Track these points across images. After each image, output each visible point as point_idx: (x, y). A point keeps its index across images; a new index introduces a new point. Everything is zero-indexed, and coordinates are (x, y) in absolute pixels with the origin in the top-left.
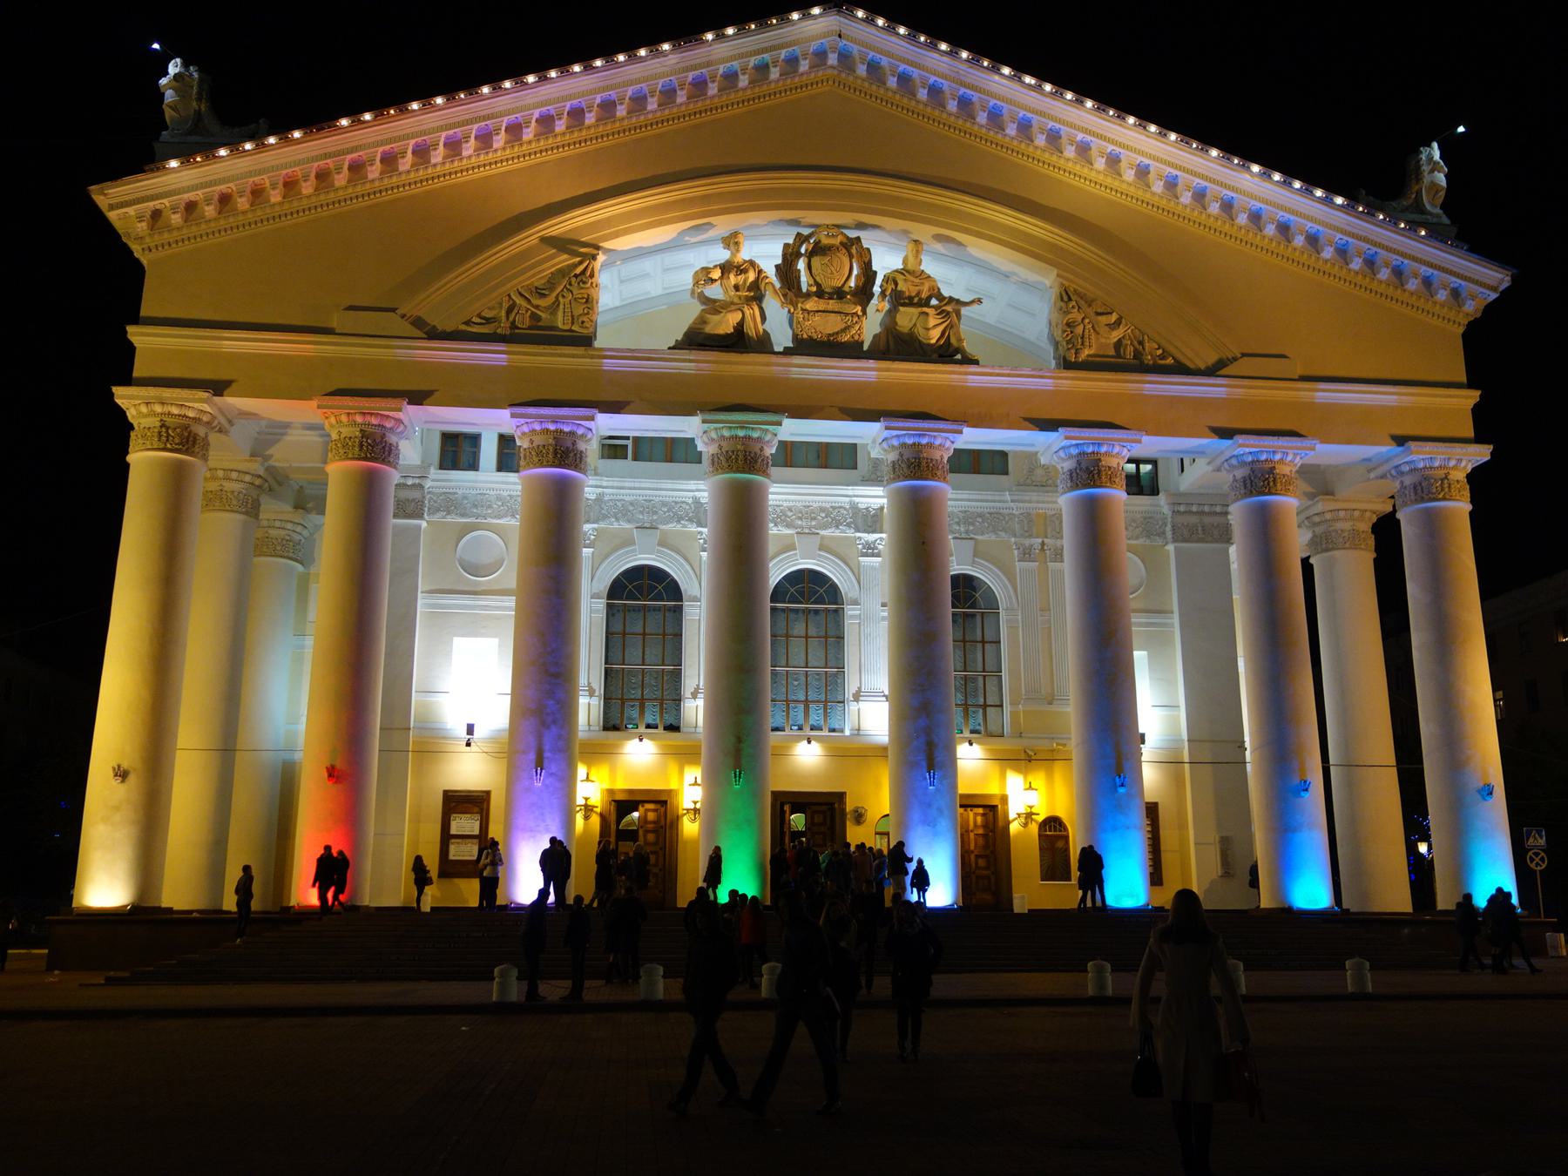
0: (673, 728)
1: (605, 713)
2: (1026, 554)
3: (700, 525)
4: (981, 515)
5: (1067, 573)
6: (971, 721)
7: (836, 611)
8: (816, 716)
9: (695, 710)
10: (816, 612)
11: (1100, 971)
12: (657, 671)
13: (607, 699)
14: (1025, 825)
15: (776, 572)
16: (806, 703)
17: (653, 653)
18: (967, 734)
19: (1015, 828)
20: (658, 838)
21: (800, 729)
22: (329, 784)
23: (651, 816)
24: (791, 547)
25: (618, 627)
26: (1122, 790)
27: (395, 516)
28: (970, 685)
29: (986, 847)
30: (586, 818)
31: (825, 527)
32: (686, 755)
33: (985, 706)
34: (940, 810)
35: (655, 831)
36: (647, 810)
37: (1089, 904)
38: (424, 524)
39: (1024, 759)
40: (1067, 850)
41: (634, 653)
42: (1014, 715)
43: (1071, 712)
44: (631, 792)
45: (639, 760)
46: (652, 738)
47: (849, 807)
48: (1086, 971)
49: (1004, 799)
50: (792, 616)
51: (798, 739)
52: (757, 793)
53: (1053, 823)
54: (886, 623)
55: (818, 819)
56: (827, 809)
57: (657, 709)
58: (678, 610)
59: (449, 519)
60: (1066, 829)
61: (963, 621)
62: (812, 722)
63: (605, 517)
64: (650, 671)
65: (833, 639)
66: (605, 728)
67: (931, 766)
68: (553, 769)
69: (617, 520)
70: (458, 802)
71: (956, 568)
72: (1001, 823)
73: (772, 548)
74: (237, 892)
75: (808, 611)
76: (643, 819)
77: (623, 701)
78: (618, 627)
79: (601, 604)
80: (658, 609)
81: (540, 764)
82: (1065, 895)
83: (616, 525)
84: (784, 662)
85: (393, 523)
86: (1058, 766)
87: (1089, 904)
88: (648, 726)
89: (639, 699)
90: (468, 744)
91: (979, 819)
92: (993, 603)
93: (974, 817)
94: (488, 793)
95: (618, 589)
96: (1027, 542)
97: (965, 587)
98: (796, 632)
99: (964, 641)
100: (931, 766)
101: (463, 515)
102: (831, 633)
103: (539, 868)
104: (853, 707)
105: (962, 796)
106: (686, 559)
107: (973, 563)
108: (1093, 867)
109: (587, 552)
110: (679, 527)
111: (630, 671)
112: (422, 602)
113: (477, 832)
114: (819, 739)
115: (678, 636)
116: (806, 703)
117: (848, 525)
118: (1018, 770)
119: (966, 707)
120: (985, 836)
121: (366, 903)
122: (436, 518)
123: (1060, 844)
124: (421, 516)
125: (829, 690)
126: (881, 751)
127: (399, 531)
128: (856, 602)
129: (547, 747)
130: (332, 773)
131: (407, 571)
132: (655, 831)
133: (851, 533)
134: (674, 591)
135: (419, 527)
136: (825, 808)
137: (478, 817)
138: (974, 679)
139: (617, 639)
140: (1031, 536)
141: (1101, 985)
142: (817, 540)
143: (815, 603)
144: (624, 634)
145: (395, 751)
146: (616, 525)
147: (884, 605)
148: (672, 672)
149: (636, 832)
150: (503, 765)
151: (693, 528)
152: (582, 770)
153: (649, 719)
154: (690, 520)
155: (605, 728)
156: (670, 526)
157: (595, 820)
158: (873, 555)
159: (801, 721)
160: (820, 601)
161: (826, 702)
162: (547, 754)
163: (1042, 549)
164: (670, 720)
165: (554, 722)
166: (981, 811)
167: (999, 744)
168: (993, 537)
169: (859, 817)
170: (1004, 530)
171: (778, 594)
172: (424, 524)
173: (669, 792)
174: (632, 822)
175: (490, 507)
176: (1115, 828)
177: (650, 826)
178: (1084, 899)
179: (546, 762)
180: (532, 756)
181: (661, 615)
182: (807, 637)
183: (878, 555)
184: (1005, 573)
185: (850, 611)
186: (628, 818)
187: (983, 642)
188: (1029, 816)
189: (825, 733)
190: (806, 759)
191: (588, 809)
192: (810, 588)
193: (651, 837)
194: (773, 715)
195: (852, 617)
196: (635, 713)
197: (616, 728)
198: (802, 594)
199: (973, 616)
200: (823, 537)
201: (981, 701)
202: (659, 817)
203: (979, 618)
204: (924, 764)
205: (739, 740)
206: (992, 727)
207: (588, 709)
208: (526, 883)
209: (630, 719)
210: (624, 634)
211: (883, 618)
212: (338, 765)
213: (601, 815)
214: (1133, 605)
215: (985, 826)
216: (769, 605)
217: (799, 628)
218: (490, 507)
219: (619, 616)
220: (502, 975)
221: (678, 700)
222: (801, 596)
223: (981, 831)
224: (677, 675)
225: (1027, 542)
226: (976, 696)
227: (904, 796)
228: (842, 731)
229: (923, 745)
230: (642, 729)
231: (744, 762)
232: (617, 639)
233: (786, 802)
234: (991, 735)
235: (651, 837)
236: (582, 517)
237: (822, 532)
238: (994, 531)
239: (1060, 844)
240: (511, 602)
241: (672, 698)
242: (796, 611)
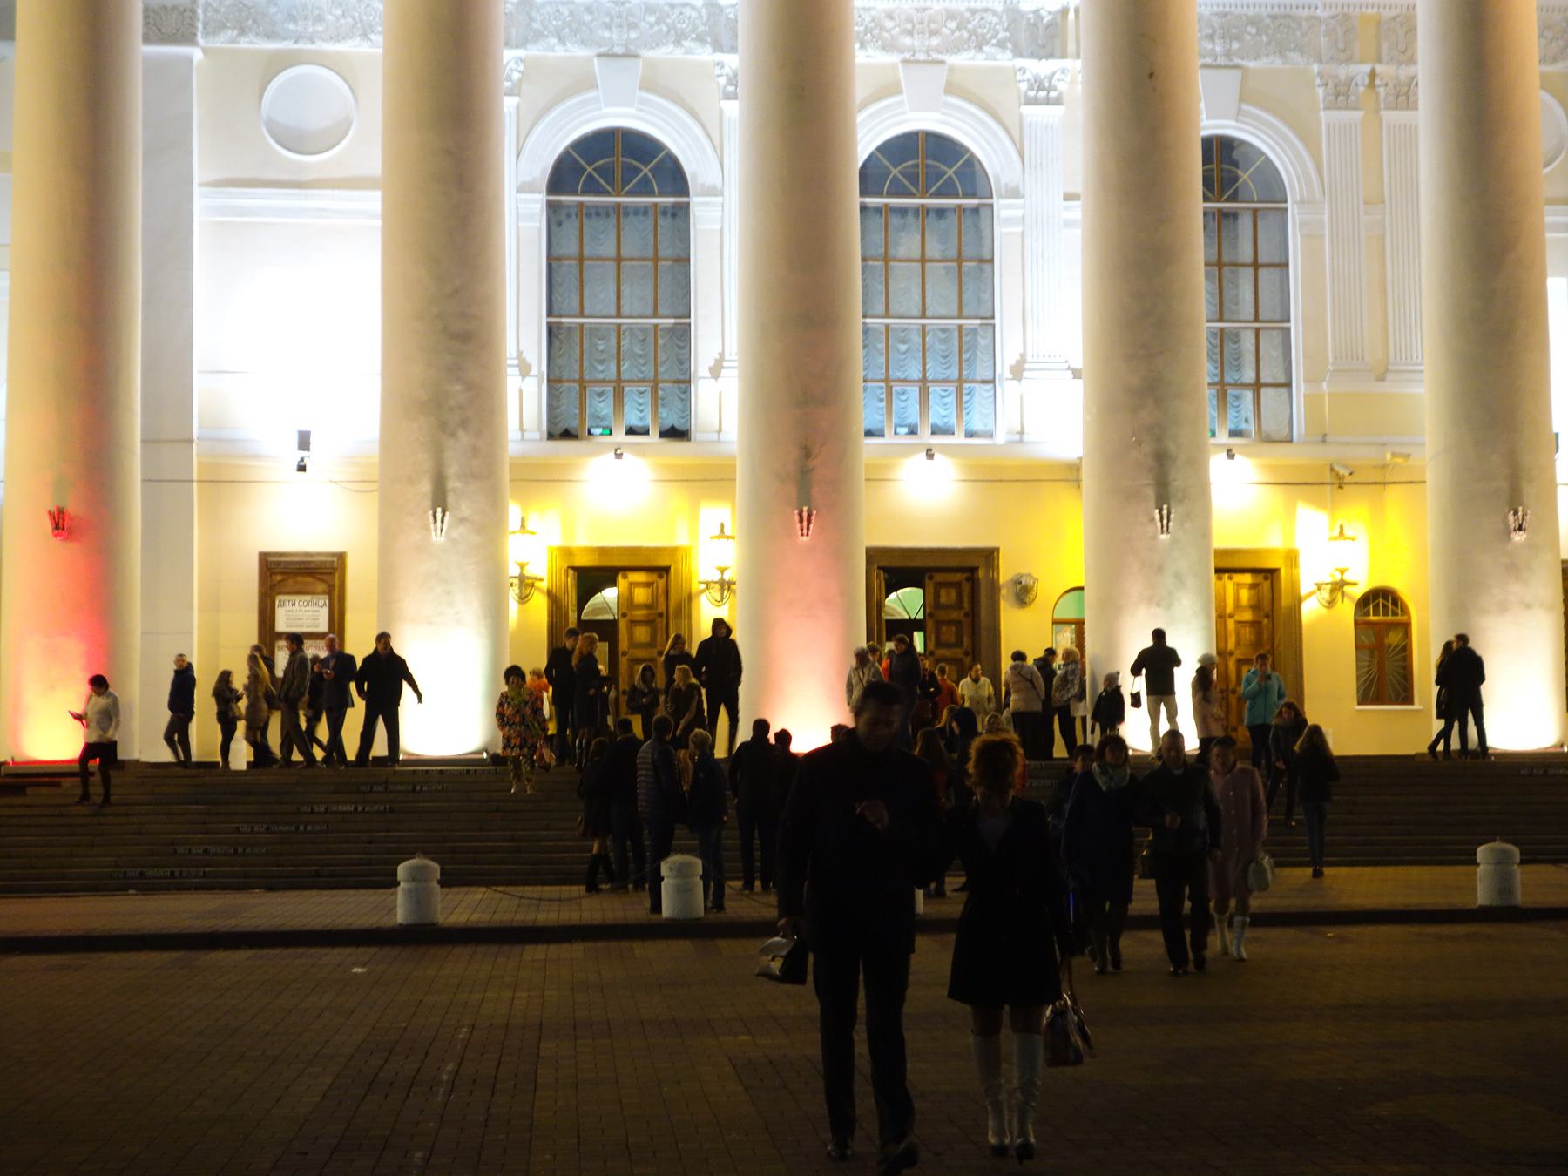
0: (676, 433)
1: (551, 408)
2: (1341, 95)
3: (718, 47)
4: (1254, 21)
5: (1423, 133)
6: (1231, 413)
7: (976, 210)
8: (941, 408)
9: (722, 399)
10: (941, 212)
11: (1502, 860)
12: (643, 329)
13: (554, 382)
14: (1331, 603)
15: (870, 132)
16: (924, 383)
17: (637, 293)
18: (1223, 438)
19: (1311, 611)
20: (654, 634)
21: (913, 431)
22: (56, 543)
23: (641, 595)
24: (893, 89)
25: (570, 247)
26: (1518, 537)
27: (147, 40)
28: (1229, 347)
29: (1257, 643)
30: (523, 599)
31: (958, 48)
32: (709, 480)
33: (1257, 386)
34: (1178, 577)
35: (649, 622)
36: (632, 585)
37: (1455, 744)
38: (197, 54)
39: (1334, 482)
40: (1405, 651)
41: (601, 293)
42: (1312, 402)
43: (1423, 395)
44: (603, 551)
45: (614, 498)
46: (640, 451)
47: (1005, 574)
48: (1475, 863)
49: (1292, 557)
50: (895, 221)
51: (910, 450)
52: (838, 553)
53: (1381, 600)
54: (1078, 232)
55: (948, 596)
56: (960, 584)
57: (648, 398)
58: (681, 213)
59: (244, 44)
60: (1405, 611)
61: (1221, 222)
62: (934, 418)
63: (538, 36)
64: (631, 328)
65: (972, 262)
66: (551, 436)
67: (1163, 496)
68: (466, 509)
69: (562, 41)
70: (280, 574)
71: (1211, 125)
72: (1285, 601)
73: (860, 88)
74: (1438, 682)
75: (924, 212)
76: (627, 602)
77: (583, 384)
78: (570, 247)
79: (536, 203)
80: (644, 211)
81: (440, 501)
82: (1411, 729)
83: (560, 52)
84: (881, 309)
85: (142, 54)
86: (1393, 493)
87: (1455, 744)
88: (631, 431)
89: (615, 375)
90: (302, 468)
91: (1245, 595)
92: (1273, 188)
93: (1239, 590)
94: (341, 557)
95: (566, 175)
96: (1343, 72)
97: (1222, 156)
98: (902, 252)
99: (1220, 264)
100: (1163, 496)
101: (270, 36)
102: (967, 253)
103: (1194, 674)
104: (1008, 390)
105: (1221, 553)
106: (694, 115)
107: (1239, 115)
108: (1462, 674)
109: (509, 104)
110: (678, 53)
111: (594, 330)
112: (203, 204)
113: (323, 627)
114: (948, 450)
115: (683, 260)
116: (924, 383)
117: (1001, 45)
118: (1318, 502)
119: (1222, 389)
120: (1255, 624)
121: (136, 756)
122: (220, 42)
123: (1393, 638)
124: (190, 39)
125: (964, 358)
126: (1070, 473)
127: (156, 68)
128: (1015, 193)
129: (452, 470)
130: (60, 523)
131: (173, 143)
132: (649, 622)
133: (1005, 60)
134: (673, 177)
135: (189, 60)
136: (958, 577)
137: (324, 600)
138: (1236, 337)
139: (569, 269)
140: (1349, 60)
141: (1504, 884)
142: (940, 74)
143: (938, 194)
144: (581, 259)
145: (168, 483)
146: (560, 52)
147: (1068, 197)
148: (672, 330)
149: (613, 624)
150: (371, 505)
151: (705, 55)
152: (514, 510)
153: (632, 417)
154: (701, 39)
155: (551, 436)
156: (665, 53)
157: (539, 607)
158: (1048, 101)
159: (913, 416)
160: (947, 191)
161: (960, 381)
162: (453, 484)
163: (1372, 85)
164: (670, 419)
165: (464, 424)
166: (1247, 578)
167: (1283, 456)
168: (1278, 63)
169: (1023, 593)
170: (1300, 49)
171: (870, 178)
172: (197, 54)
173: (673, 551)
174: (606, 608)
175: (319, 19)
176: (1503, 608)
177: (640, 614)
178: (1445, 734)
179: (451, 499)
180: (426, 487)
181: (650, 221)
182: (923, 260)
183: (1058, 101)
184: (1303, 139)
185: (1004, 209)
186: (597, 599)
187: (1256, 265)
188: (1338, 587)
189: (959, 439)
190: (919, 495)
191: (526, 585)
192: (930, 170)
193: (642, 634)
194: (867, 410)
195: (1009, 221)
196: (605, 407)
197: (567, 435)
198: (913, 179)
199: (1234, 215)
200: (952, 69)
201: (1249, 376)
202: (655, 597)
203: (1245, 223)
204: (1150, 493)
205: (807, 453)
206: (1269, 425)
207: (523, 398)
208: (447, 720)
209: (598, 418)
210: (581, 259)
211: (1068, 224)
212: (73, 507)
213: (550, 595)
214: (1548, 190)
215: (1256, 607)
216: (856, 200)
217: (908, 244)
218: (319, 19)
219: (570, 228)
220: (415, 876)
221: (684, 383)
222: (914, 183)
223: (1247, 616)
224: (682, 335)
225: (1343, 72)
226: (1239, 368)
227: (1114, 553)
228: (990, 435)
229: (1149, 461)
230: (620, 436)
231: (816, 492)
232: (569, 269)
233: (894, 569)
234: (1269, 440)
235: (642, 634)
236: (501, 36)
237: (952, 59)
238: (1281, 52)
239: (1393, 638)
240: (373, 201)
241: (678, 383)
242: (903, 211)
